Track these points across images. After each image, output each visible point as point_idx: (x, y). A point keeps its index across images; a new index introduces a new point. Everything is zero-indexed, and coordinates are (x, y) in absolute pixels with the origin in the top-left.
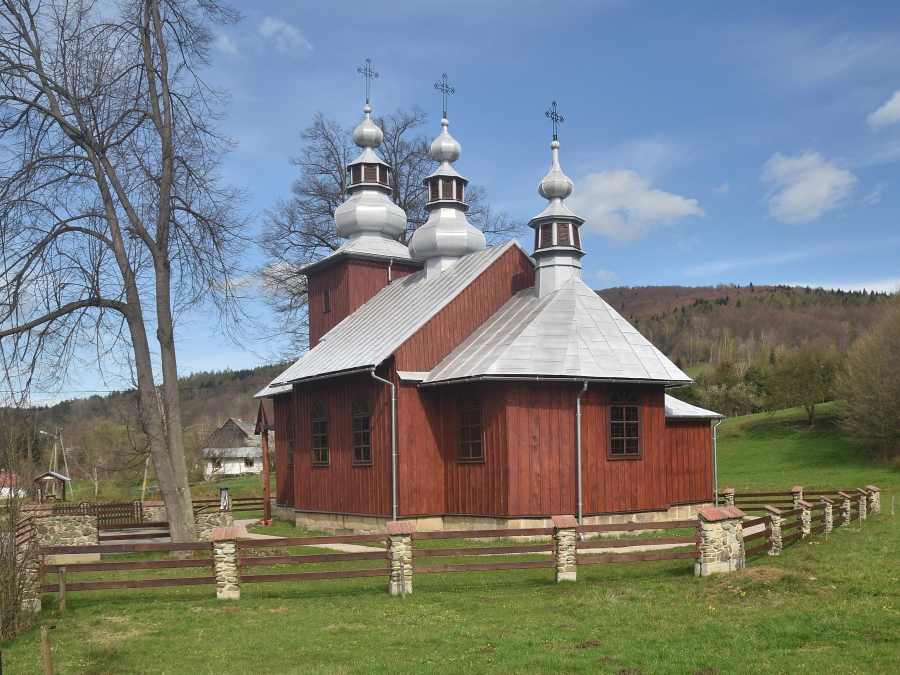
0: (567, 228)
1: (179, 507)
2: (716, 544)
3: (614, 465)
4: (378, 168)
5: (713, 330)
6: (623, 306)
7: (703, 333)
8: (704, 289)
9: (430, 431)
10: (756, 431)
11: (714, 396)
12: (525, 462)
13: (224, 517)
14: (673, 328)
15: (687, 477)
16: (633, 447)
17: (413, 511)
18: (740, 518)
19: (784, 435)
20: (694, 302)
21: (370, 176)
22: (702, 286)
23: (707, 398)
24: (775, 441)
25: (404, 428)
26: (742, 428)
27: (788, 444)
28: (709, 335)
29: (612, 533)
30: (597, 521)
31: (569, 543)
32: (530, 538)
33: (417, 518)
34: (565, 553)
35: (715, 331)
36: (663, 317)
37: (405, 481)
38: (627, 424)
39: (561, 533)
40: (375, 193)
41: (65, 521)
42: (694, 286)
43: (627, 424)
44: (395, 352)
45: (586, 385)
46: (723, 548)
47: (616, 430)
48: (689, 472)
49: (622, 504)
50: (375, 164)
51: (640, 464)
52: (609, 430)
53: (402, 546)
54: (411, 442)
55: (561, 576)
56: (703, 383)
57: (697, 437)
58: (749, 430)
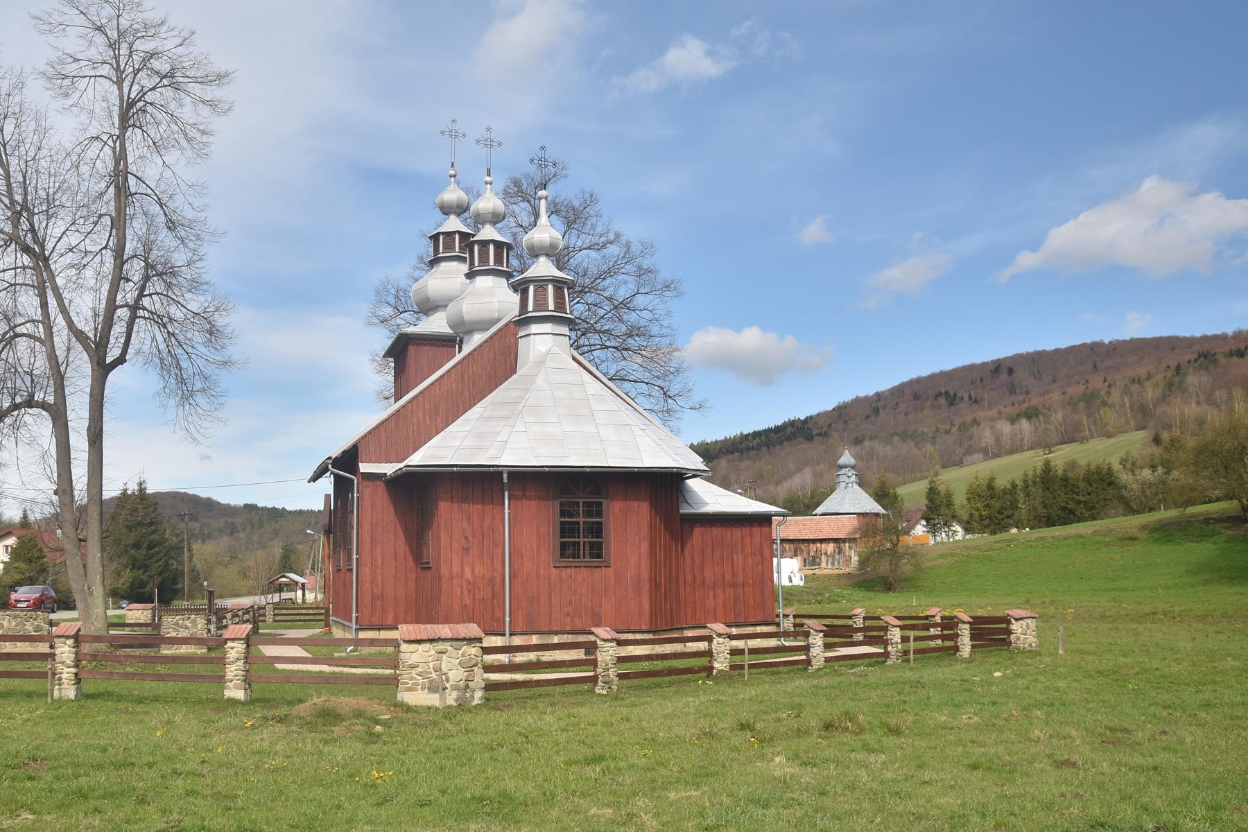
0: (546, 290)
1: (87, 606)
2: (420, 670)
3: (565, 573)
4: (457, 236)
5: (1217, 393)
6: (1095, 366)
7: (1202, 398)
8: (1215, 338)
9: (398, 526)
10: (1165, 532)
11: (1144, 483)
12: (456, 568)
13: (195, 621)
14: (1158, 392)
15: (729, 591)
16: (597, 551)
17: (376, 620)
18: (480, 640)
19: (1203, 537)
20: (1196, 356)
21: (449, 246)
22: (1210, 333)
23: (1135, 486)
24: (1187, 545)
25: (366, 526)
26: (1144, 528)
27: (1203, 550)
28: (1211, 401)
29: (383, 649)
30: (535, 640)
31: (236, 655)
32: (373, 650)
33: (379, 630)
34: (233, 668)
35: (1220, 395)
36: (1148, 379)
37: (366, 586)
38: (578, 523)
39: (230, 644)
40: (455, 263)
41: (15, 617)
42: (1198, 334)
43: (578, 523)
44: (358, 441)
45: (505, 476)
46: (434, 675)
47: (567, 529)
48: (734, 585)
49: (577, 621)
50: (454, 233)
51: (610, 572)
52: (558, 529)
53: (66, 648)
54: (373, 542)
55: (228, 694)
56: (1128, 466)
57: (748, 540)
58: (1155, 530)
